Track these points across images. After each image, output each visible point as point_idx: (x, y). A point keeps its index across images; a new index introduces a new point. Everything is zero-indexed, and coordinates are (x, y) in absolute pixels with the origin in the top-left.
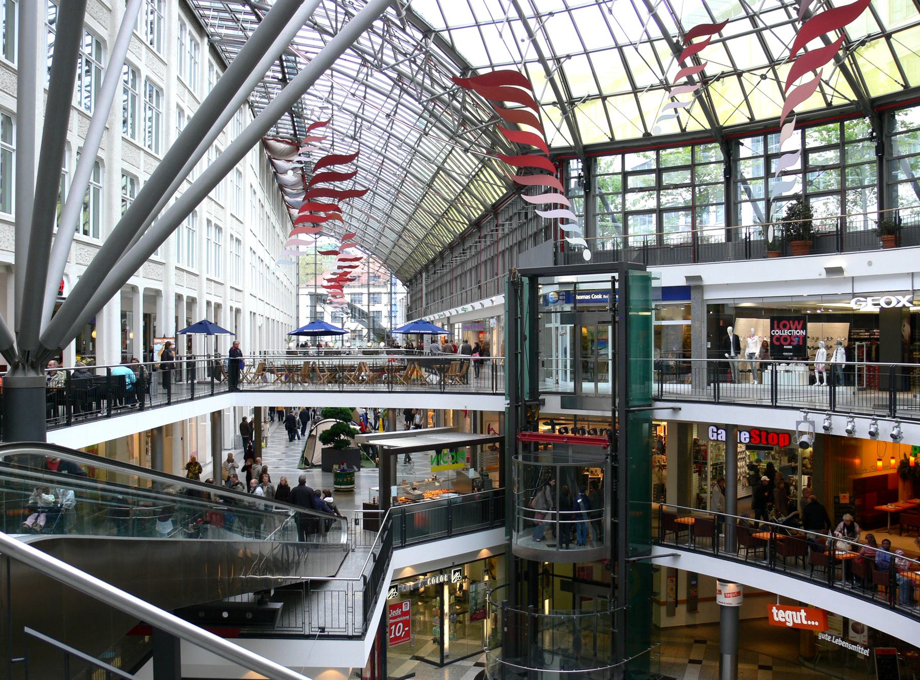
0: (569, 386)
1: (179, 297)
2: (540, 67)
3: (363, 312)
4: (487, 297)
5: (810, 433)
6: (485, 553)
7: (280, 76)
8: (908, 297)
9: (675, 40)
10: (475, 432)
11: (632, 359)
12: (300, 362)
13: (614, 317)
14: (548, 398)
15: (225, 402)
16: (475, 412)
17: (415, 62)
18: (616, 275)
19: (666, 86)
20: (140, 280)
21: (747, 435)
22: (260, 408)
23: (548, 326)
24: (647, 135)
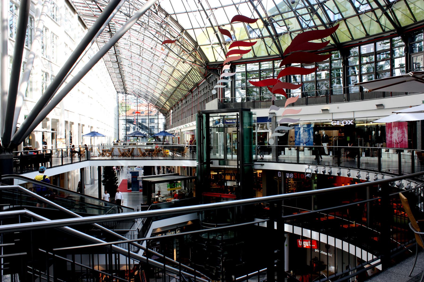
0: (222, 156)
1: (66, 122)
2: (212, 29)
3: (147, 127)
4: (187, 123)
5: (310, 173)
6: (190, 223)
7: (108, 30)
8: (352, 121)
9: (264, 19)
10: (188, 175)
11: (245, 146)
12: (154, 147)
13: (237, 129)
14: (214, 161)
15: (86, 164)
16: (188, 167)
17: (162, 27)
18: (238, 113)
19: (345, 19)
20: (50, 116)
21: (292, 175)
22: (160, 166)
23: (254, 131)
24: (255, 56)
